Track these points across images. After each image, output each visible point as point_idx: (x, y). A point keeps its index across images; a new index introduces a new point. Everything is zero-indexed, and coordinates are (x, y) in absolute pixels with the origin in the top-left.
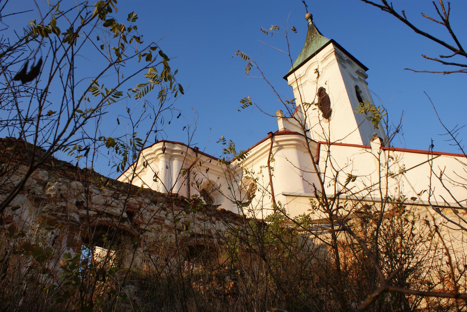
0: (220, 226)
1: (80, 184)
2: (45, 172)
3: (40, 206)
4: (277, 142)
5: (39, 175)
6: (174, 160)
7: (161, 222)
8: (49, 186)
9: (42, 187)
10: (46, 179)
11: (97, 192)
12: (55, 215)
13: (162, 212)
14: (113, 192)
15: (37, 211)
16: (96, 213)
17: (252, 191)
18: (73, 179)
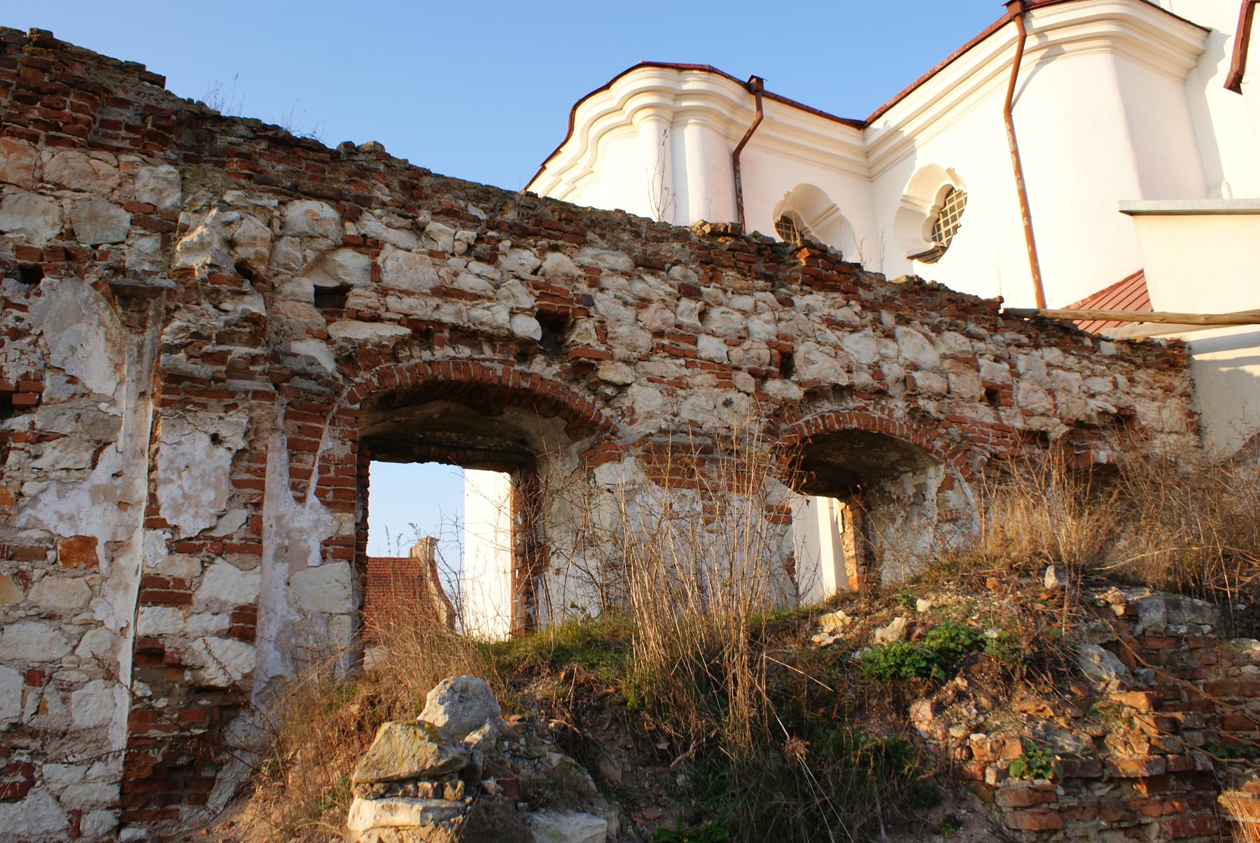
0: (914, 346)
1: (327, 211)
2: (165, 169)
3: (149, 323)
4: (1041, 33)
5: (139, 185)
6: (686, 125)
7: (684, 346)
8: (185, 229)
9: (158, 236)
10: (171, 199)
11: (404, 238)
12: (219, 358)
13: (685, 303)
14: (470, 234)
15: (141, 346)
16: (406, 331)
17: (945, 214)
18: (296, 192)
